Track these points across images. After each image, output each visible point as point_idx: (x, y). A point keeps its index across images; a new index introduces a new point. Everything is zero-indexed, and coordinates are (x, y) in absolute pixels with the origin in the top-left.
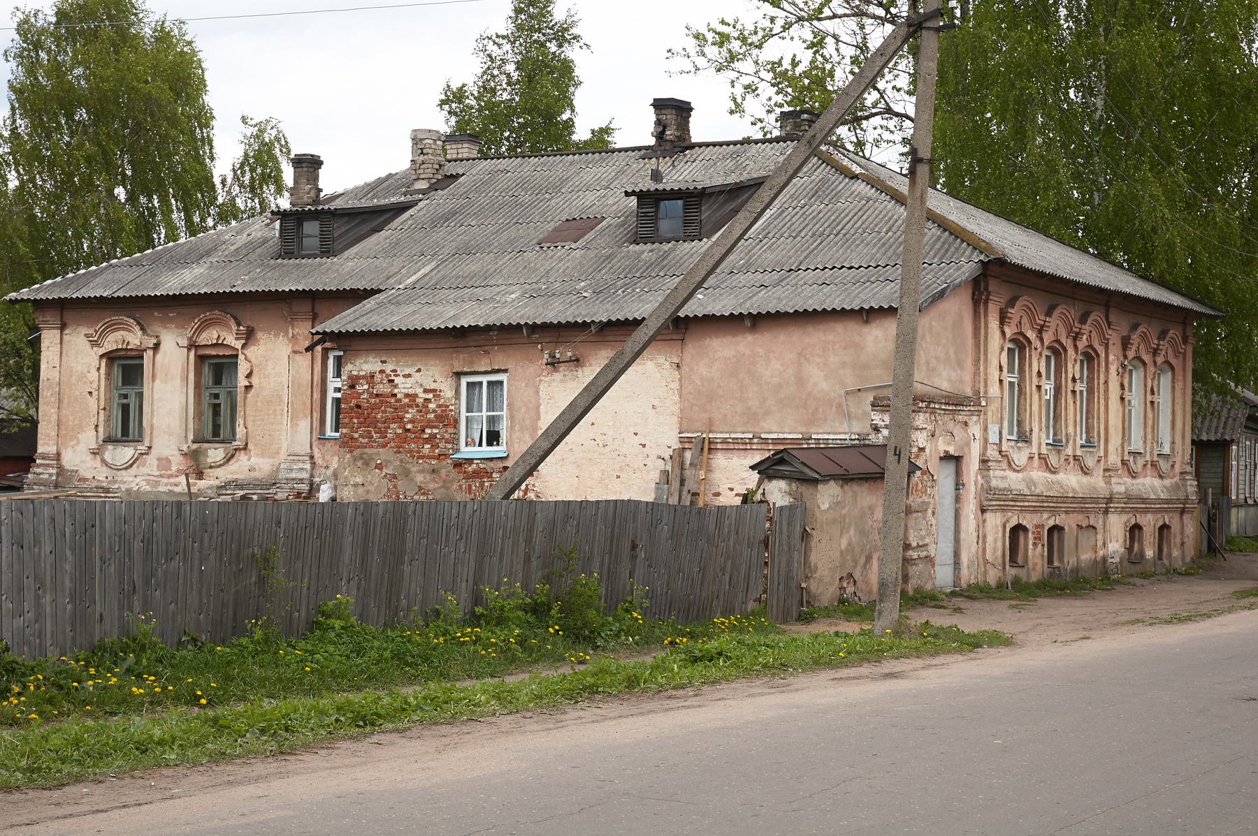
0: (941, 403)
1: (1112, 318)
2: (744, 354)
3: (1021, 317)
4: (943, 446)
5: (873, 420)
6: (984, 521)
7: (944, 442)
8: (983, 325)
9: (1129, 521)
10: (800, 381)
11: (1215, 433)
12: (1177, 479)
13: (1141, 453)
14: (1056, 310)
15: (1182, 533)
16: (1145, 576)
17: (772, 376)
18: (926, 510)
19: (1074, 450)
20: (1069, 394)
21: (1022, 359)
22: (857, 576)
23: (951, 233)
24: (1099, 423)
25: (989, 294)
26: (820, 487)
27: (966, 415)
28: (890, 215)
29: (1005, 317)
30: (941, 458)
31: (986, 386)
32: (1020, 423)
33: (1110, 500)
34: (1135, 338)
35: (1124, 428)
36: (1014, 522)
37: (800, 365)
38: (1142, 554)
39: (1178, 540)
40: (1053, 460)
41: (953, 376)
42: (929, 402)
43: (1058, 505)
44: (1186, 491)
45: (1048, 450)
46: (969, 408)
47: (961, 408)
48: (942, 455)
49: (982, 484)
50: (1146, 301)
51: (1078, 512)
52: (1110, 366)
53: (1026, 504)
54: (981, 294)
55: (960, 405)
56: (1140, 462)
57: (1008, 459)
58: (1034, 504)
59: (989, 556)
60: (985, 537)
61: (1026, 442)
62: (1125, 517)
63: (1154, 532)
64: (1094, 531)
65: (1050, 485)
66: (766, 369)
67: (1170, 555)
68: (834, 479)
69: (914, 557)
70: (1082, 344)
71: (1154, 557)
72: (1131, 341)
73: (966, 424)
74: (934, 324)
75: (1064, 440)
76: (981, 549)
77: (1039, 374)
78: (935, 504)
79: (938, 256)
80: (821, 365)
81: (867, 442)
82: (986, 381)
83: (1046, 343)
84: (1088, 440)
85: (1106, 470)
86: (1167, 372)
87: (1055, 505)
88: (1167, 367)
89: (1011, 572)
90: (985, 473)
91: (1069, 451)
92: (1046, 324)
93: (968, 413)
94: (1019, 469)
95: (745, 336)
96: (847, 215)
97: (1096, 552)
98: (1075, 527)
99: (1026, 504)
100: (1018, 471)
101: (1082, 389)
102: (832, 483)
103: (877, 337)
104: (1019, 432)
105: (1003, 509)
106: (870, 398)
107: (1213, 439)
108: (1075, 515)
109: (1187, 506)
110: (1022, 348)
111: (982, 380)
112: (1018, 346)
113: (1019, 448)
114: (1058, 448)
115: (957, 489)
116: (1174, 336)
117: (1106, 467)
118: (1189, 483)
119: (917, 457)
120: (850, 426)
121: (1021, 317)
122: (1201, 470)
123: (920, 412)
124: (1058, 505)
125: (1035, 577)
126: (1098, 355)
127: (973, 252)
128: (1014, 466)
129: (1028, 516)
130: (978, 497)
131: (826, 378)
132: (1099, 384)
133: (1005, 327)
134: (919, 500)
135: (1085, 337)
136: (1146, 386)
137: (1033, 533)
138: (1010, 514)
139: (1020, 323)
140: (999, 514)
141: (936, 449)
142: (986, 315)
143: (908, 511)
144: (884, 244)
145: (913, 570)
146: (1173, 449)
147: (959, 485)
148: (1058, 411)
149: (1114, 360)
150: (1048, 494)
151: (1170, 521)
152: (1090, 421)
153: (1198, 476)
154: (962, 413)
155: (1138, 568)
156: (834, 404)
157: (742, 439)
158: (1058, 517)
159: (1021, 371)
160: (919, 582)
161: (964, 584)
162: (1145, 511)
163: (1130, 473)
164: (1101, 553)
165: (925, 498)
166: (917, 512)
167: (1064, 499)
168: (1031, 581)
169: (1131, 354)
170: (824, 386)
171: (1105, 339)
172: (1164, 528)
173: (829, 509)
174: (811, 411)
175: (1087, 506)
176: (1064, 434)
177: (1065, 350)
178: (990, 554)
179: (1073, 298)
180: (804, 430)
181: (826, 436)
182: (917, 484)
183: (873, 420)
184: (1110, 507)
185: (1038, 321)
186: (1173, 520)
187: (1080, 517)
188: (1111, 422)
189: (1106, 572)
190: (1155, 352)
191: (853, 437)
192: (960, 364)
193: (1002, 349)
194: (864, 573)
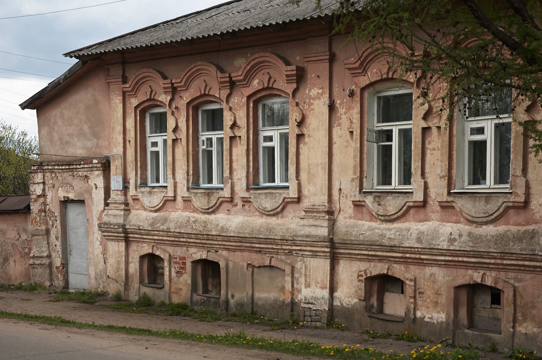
41: (89, 144)
46: (82, 166)
47: (75, 167)
178: (112, 272)
194: (4, 268)
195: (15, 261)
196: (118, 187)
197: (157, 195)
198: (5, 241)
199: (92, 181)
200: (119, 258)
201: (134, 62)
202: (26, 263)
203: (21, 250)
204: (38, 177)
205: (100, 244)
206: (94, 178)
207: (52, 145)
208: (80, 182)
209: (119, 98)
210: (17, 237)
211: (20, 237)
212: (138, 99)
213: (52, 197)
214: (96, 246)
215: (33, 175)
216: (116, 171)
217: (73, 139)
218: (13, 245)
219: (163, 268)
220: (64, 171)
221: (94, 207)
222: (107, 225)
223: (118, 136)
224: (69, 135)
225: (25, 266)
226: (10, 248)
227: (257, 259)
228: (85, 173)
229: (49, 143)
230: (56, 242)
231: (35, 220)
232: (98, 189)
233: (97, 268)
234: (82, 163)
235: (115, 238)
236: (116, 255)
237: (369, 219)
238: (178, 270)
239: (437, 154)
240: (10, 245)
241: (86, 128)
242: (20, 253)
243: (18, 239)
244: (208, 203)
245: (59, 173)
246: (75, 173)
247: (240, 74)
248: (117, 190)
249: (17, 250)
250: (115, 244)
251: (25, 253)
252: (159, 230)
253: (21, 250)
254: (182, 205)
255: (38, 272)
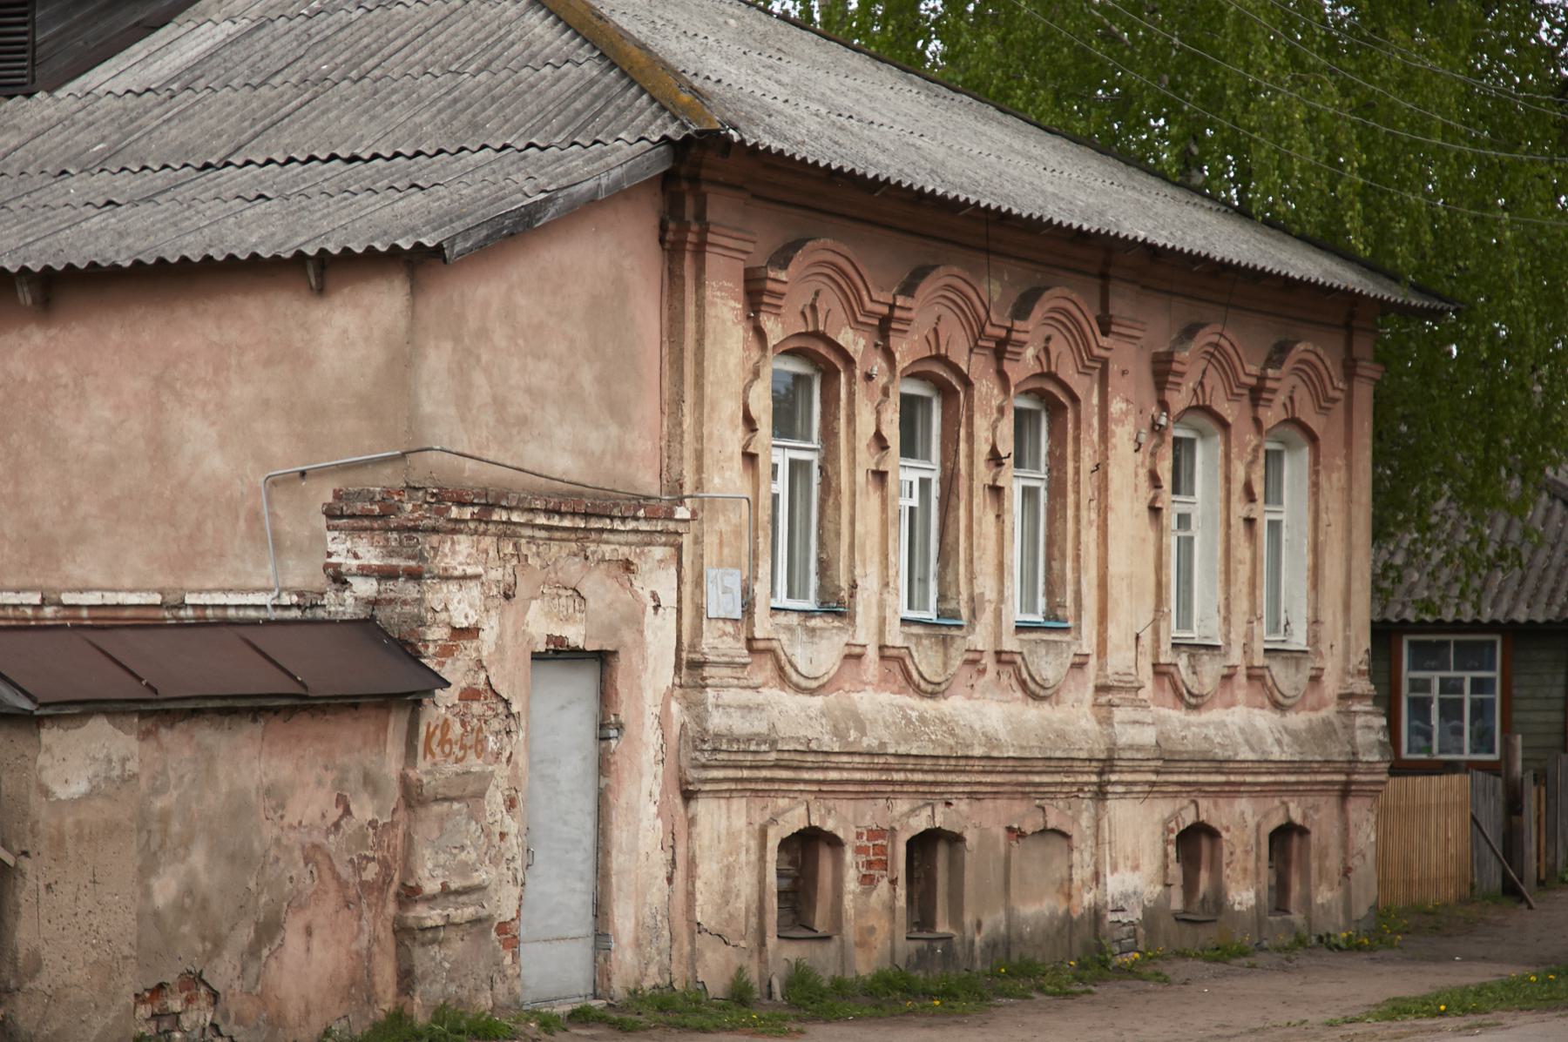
0: (532, 510)
1: (1118, 307)
2: (24, 381)
3: (817, 293)
4: (540, 624)
5: (330, 555)
6: (692, 822)
7: (548, 614)
8: (691, 309)
9: (1175, 816)
10: (160, 450)
11: (1549, 604)
12: (1329, 712)
13: (1217, 647)
14: (929, 279)
15: (1345, 845)
16: (1224, 954)
17: (91, 440)
18: (480, 795)
19: (998, 636)
20: (980, 496)
21: (829, 402)
22: (223, 974)
23: (624, 74)
24: (1077, 570)
25: (704, 230)
26: (49, 735)
27: (627, 544)
28: (502, 32)
29: (762, 292)
30: (537, 657)
31: (699, 469)
32: (824, 567)
33: (1107, 764)
34: (1190, 359)
35: (1159, 585)
36: (794, 821)
37: (160, 407)
38: (1218, 898)
39: (1334, 863)
40: (926, 662)
41: (595, 440)
42: (489, 507)
43: (942, 777)
44: (1352, 741)
45: (908, 636)
46: (631, 525)
47: (607, 524)
48: (541, 648)
49: (683, 726)
50: (1223, 270)
51: (1011, 796)
52: (1112, 427)
53: (833, 775)
54: (684, 228)
55: (600, 516)
56: (1211, 670)
57: (777, 660)
58: (858, 776)
59: (705, 912)
60: (692, 864)
61: (839, 615)
62: (1163, 808)
63: (1258, 843)
64: (1064, 843)
65: (909, 725)
66: (78, 421)
67: (1307, 901)
68: (106, 713)
69: (429, 923)
70: (1025, 364)
71: (1258, 906)
72: (1175, 366)
73: (627, 566)
74: (521, 300)
75: (965, 612)
76: (680, 897)
77: (880, 441)
78: (514, 777)
79: (571, 128)
80: (210, 407)
81: (320, 614)
82: (699, 456)
83: (903, 361)
84: (1051, 614)
85: (1101, 689)
86: (1300, 447)
87: (930, 777)
88: (1294, 434)
89: (785, 954)
90: (694, 695)
91: (980, 638)
92: (898, 313)
93: (632, 538)
94: (814, 684)
95: (26, 331)
96: (402, 34)
97: (1069, 897)
98: (1001, 833)
99: (833, 775)
100: (812, 692)
101: (926, 475)
102: (99, 726)
103: (345, 331)
104: (822, 589)
105: (755, 790)
106: (324, 493)
107: (1540, 618)
108: (1001, 803)
109: (1356, 777)
110: (1055, 410)
111: (688, 453)
112: (818, 370)
113: (813, 630)
114: (944, 631)
115: (604, 738)
116: (1312, 358)
117: (1101, 681)
118: (1359, 721)
119: (446, 651)
120: (280, 569)
121: (817, 293)
122: (1515, 692)
123: (454, 531)
124: (942, 777)
125: (864, 966)
126: (1075, 399)
127: (656, 117)
128: (795, 677)
129: (846, 807)
130: (671, 759)
131: (223, 443)
132: (1077, 471)
133: (763, 318)
134: (451, 768)
135: (1030, 352)
136: (1228, 479)
137: (859, 850)
138: (783, 802)
139: (813, 308)
140: (739, 804)
141: (519, 632)
142: (700, 284)
143: (413, 797)
144: (455, 101)
145: (424, 958)
146: (1314, 639)
147: (606, 727)
148: (950, 539)
149: (1126, 414)
150: (902, 750)
151: (1305, 817)
152: (1056, 565)
153: (1387, 701)
154: (612, 537)
155: (1207, 935)
156: (242, 515)
157: (15, 606)
158: (940, 808)
159: (829, 434)
160: (452, 988)
161: (618, 988)
162: (1231, 791)
163: (1180, 696)
164: (1088, 898)
165: (475, 764)
166: (446, 799)
167: (959, 761)
168: (850, 976)
169: (1179, 399)
170: (216, 463)
171: (1093, 358)
172: (1284, 838)
173: (88, 796)
174: (185, 531)
175: (1037, 779)
176: (964, 596)
177: (967, 383)
178: (709, 909)
179: (987, 251)
180: (167, 581)
181: (220, 599)
182: (446, 725)
183: (330, 555)
184: (1109, 783)
185: (869, 306)
186: (1320, 817)
187: (1019, 807)
188: (1116, 567)
189: (1101, 949)
190: (1257, 394)
191: (286, 600)
192: (617, 410)
193: (756, 374)
194: (253, 970)
195: (309, 931)
196: (730, 608)
197: (828, 638)
198: (278, 841)
199: (644, 581)
200: (731, 854)
201: (1017, 258)
202: (360, 929)
203: (345, 872)
204: (454, 553)
205: (659, 814)
206: (651, 571)
207: (463, 420)
208: (609, 582)
209: (732, 303)
210: (335, 813)
211: (347, 812)
212: (783, 323)
213: (501, 636)
214: (645, 824)
215: (435, 539)
216: (721, 553)
217: (543, 408)
218: (312, 854)
219: (781, 874)
220: (558, 535)
221: (646, 678)
222: (738, 741)
223: (728, 433)
224: (529, 391)
225: (354, 947)
226: (299, 869)
227: (1023, 814)
228: (624, 551)
229: (452, 411)
230: (508, 819)
231: (444, 734)
232: (661, 610)
233: (644, 904)
234: (641, 513)
235: (733, 786)
236: (723, 844)
237: (1171, 705)
238: (864, 871)
239: (766, 536)
240: (298, 854)
241: (586, 376)
242: (342, 885)
243: (337, 825)
244: (945, 665)
245: (532, 539)
246: (592, 547)
247: (875, 297)
248: (725, 620)
249: (327, 875)
250: (719, 807)
251: (363, 884)
252: (861, 750)
253: (345, 872)
254: (876, 673)
255: (444, 959)
